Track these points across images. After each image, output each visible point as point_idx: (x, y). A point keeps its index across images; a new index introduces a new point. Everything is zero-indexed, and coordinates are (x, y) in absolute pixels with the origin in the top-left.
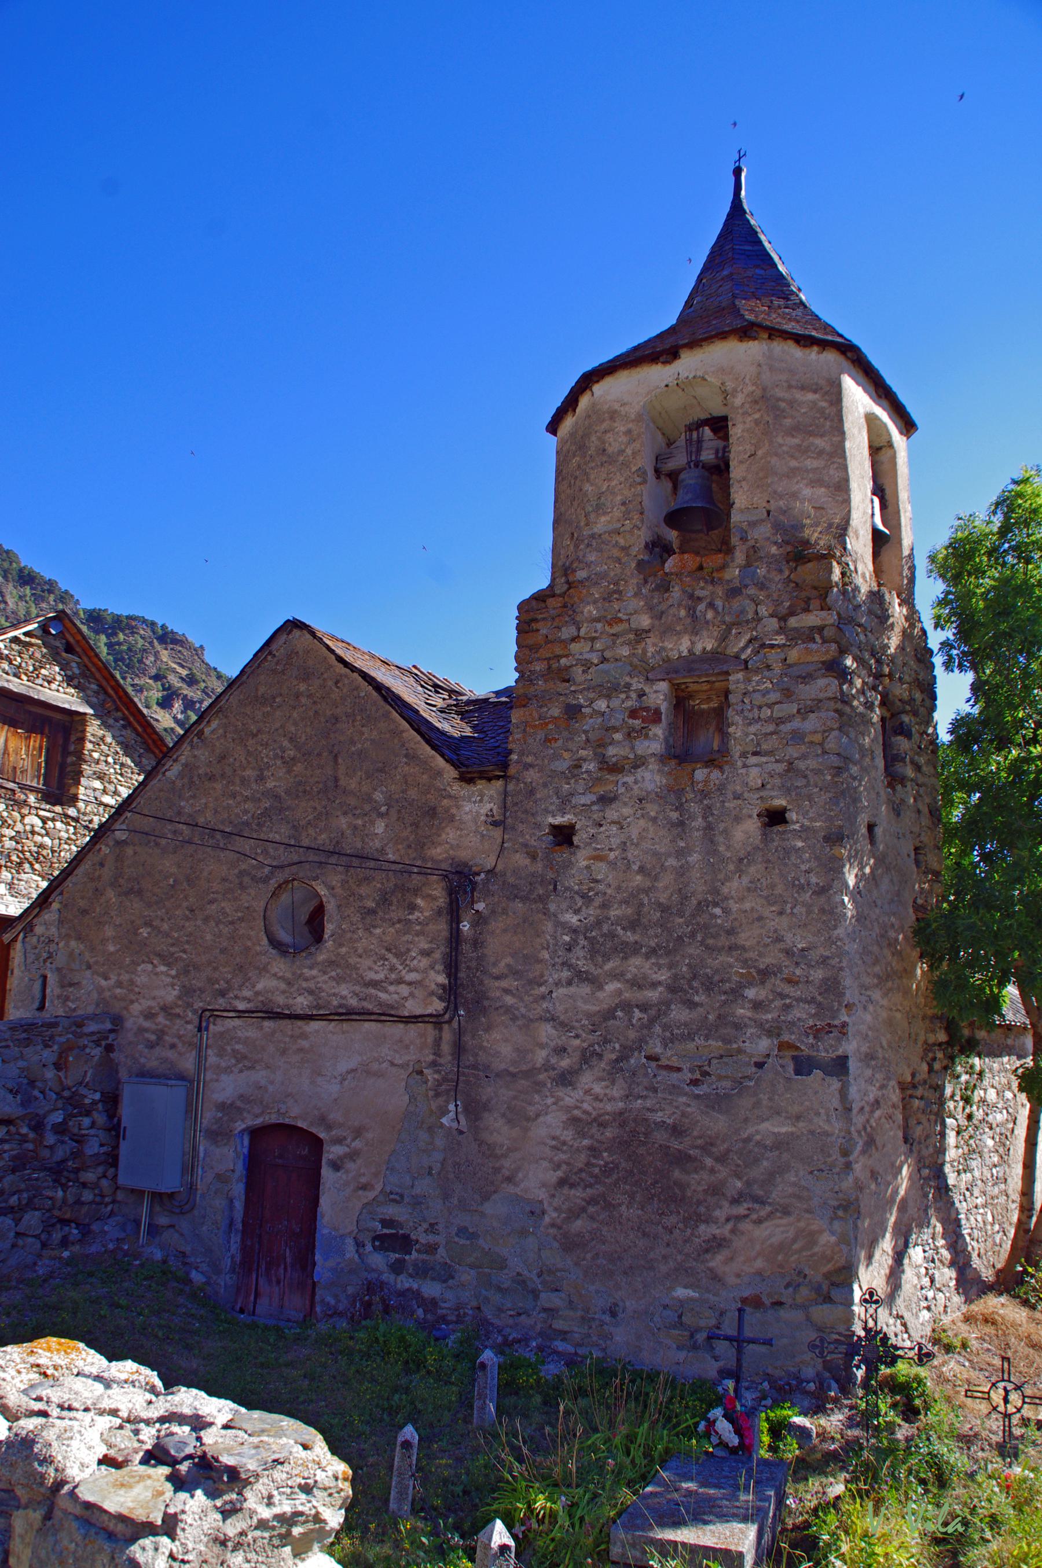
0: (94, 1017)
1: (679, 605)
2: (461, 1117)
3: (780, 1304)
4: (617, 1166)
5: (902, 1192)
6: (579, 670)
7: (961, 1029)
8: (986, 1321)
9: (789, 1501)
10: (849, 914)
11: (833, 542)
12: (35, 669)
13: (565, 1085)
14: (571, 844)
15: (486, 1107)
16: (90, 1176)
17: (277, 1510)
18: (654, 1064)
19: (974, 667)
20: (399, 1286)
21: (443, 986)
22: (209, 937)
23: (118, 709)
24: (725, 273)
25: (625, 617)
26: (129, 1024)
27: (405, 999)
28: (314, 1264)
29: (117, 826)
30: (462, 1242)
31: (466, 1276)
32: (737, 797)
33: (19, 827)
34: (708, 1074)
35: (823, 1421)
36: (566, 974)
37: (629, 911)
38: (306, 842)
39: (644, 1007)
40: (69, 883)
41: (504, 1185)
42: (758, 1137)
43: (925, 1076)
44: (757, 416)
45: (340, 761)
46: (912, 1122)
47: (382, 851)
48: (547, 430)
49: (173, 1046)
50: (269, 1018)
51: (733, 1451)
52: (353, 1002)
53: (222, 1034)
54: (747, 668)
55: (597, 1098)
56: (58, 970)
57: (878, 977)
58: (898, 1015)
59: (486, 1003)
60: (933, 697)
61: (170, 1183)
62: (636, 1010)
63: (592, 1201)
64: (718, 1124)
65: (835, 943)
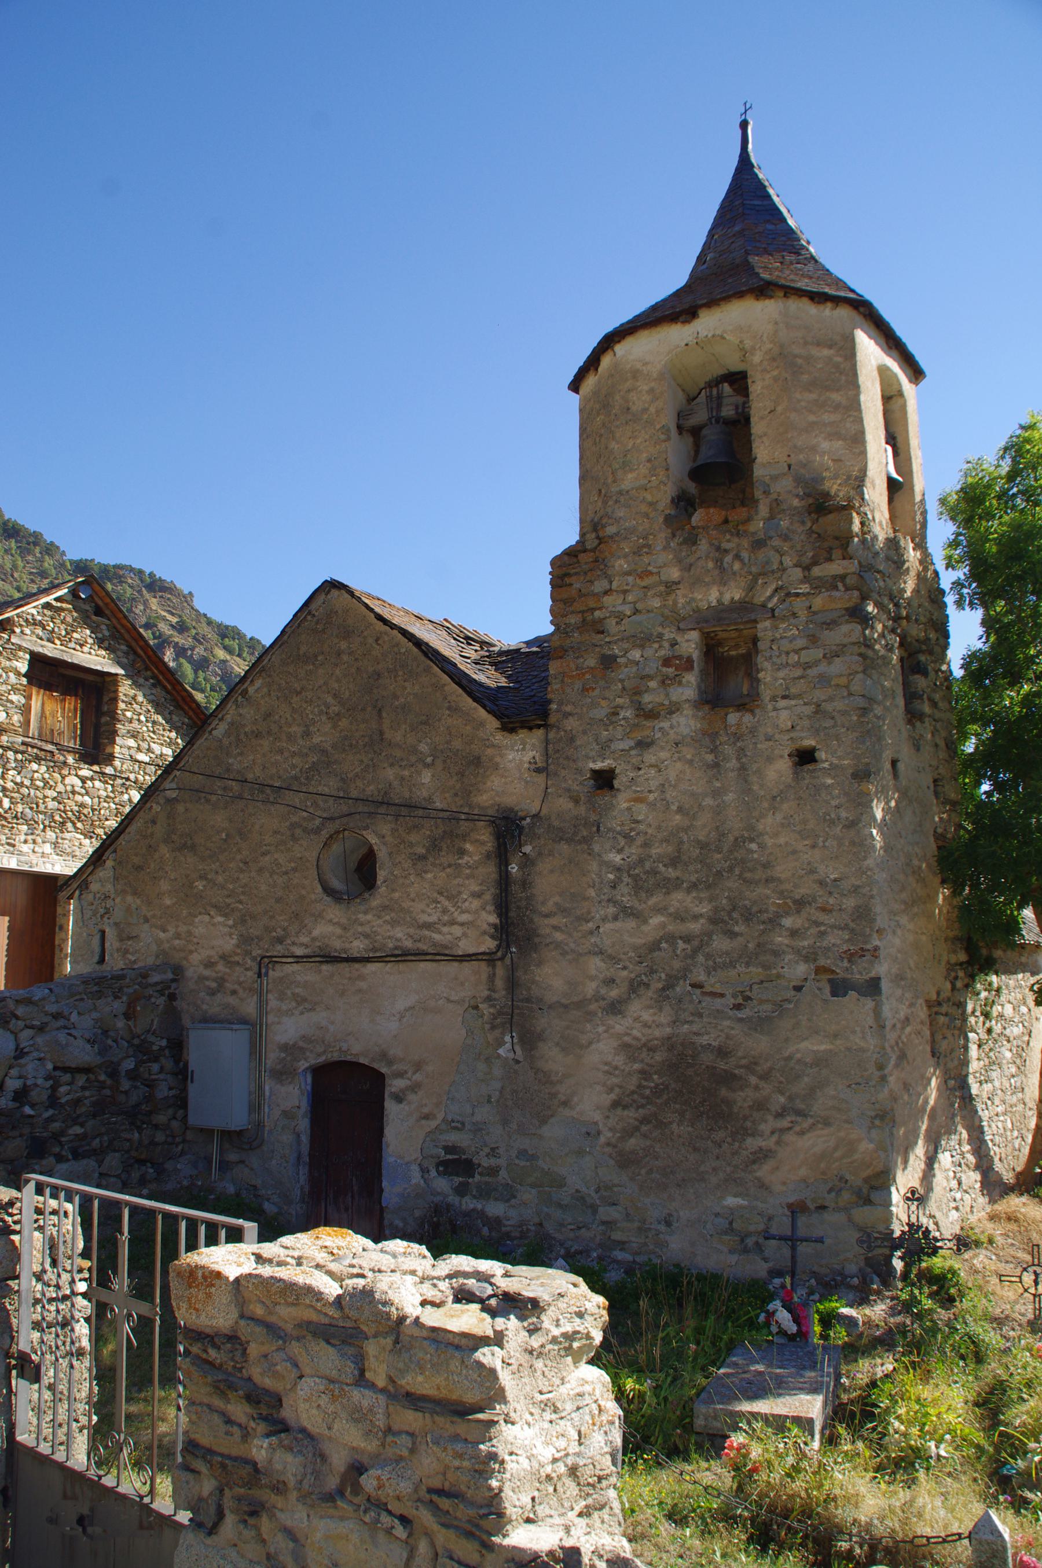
0: (155, 968)
1: (707, 557)
2: (517, 1048)
3: (822, 1208)
4: (667, 1087)
5: (932, 1102)
6: (613, 621)
7: (981, 946)
8: (1009, 1219)
9: (844, 1380)
10: (878, 846)
11: (852, 493)
12: (67, 633)
13: (615, 1014)
14: (611, 787)
15: (541, 1037)
16: (161, 1118)
17: (563, 1330)
18: (698, 991)
19: (985, 606)
20: (464, 1207)
21: (495, 926)
22: (263, 887)
23: (147, 669)
24: (737, 228)
25: (655, 570)
26: (189, 973)
27: (459, 939)
28: (382, 1191)
29: (167, 785)
30: (522, 1163)
31: (528, 1195)
32: (769, 739)
33: (60, 788)
34: (749, 998)
35: (867, 1311)
36: (611, 910)
37: (670, 849)
38: (354, 794)
39: (687, 939)
40: (122, 840)
41: (561, 1109)
42: (799, 1056)
43: (948, 994)
44: (775, 373)
45: (384, 715)
46: (938, 1037)
47: (430, 799)
48: (569, 388)
49: (234, 992)
50: (327, 962)
51: (792, 1338)
52: (408, 944)
53: (281, 979)
54: (773, 616)
55: (646, 1025)
56: (116, 924)
57: (905, 902)
58: (924, 938)
59: (537, 940)
60: (946, 635)
61: (238, 1119)
62: (680, 942)
63: (645, 1120)
64: (759, 1044)
65: (864, 873)
